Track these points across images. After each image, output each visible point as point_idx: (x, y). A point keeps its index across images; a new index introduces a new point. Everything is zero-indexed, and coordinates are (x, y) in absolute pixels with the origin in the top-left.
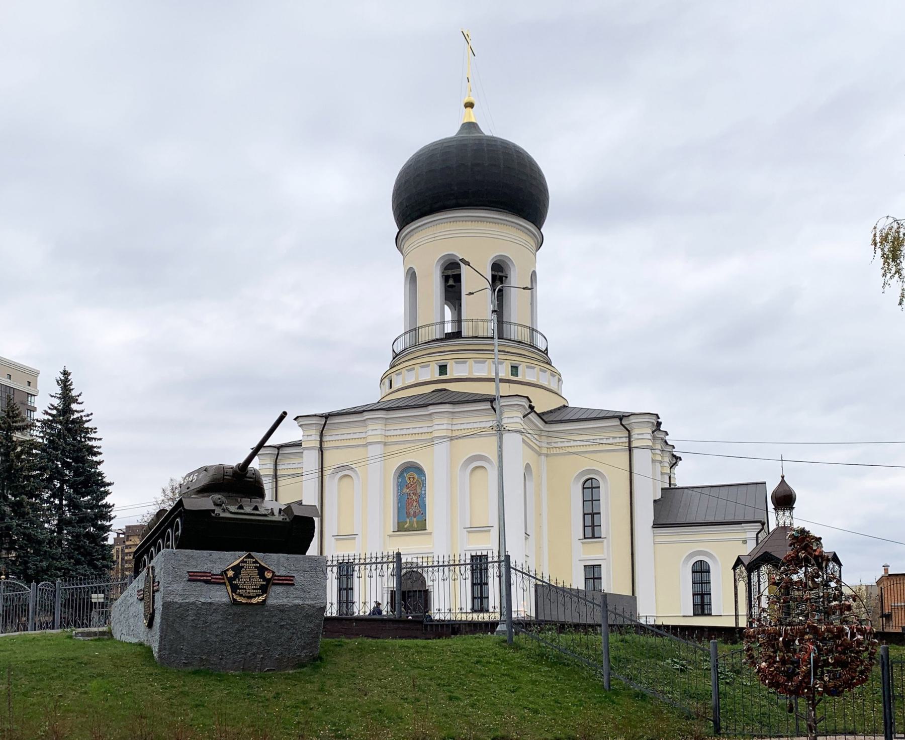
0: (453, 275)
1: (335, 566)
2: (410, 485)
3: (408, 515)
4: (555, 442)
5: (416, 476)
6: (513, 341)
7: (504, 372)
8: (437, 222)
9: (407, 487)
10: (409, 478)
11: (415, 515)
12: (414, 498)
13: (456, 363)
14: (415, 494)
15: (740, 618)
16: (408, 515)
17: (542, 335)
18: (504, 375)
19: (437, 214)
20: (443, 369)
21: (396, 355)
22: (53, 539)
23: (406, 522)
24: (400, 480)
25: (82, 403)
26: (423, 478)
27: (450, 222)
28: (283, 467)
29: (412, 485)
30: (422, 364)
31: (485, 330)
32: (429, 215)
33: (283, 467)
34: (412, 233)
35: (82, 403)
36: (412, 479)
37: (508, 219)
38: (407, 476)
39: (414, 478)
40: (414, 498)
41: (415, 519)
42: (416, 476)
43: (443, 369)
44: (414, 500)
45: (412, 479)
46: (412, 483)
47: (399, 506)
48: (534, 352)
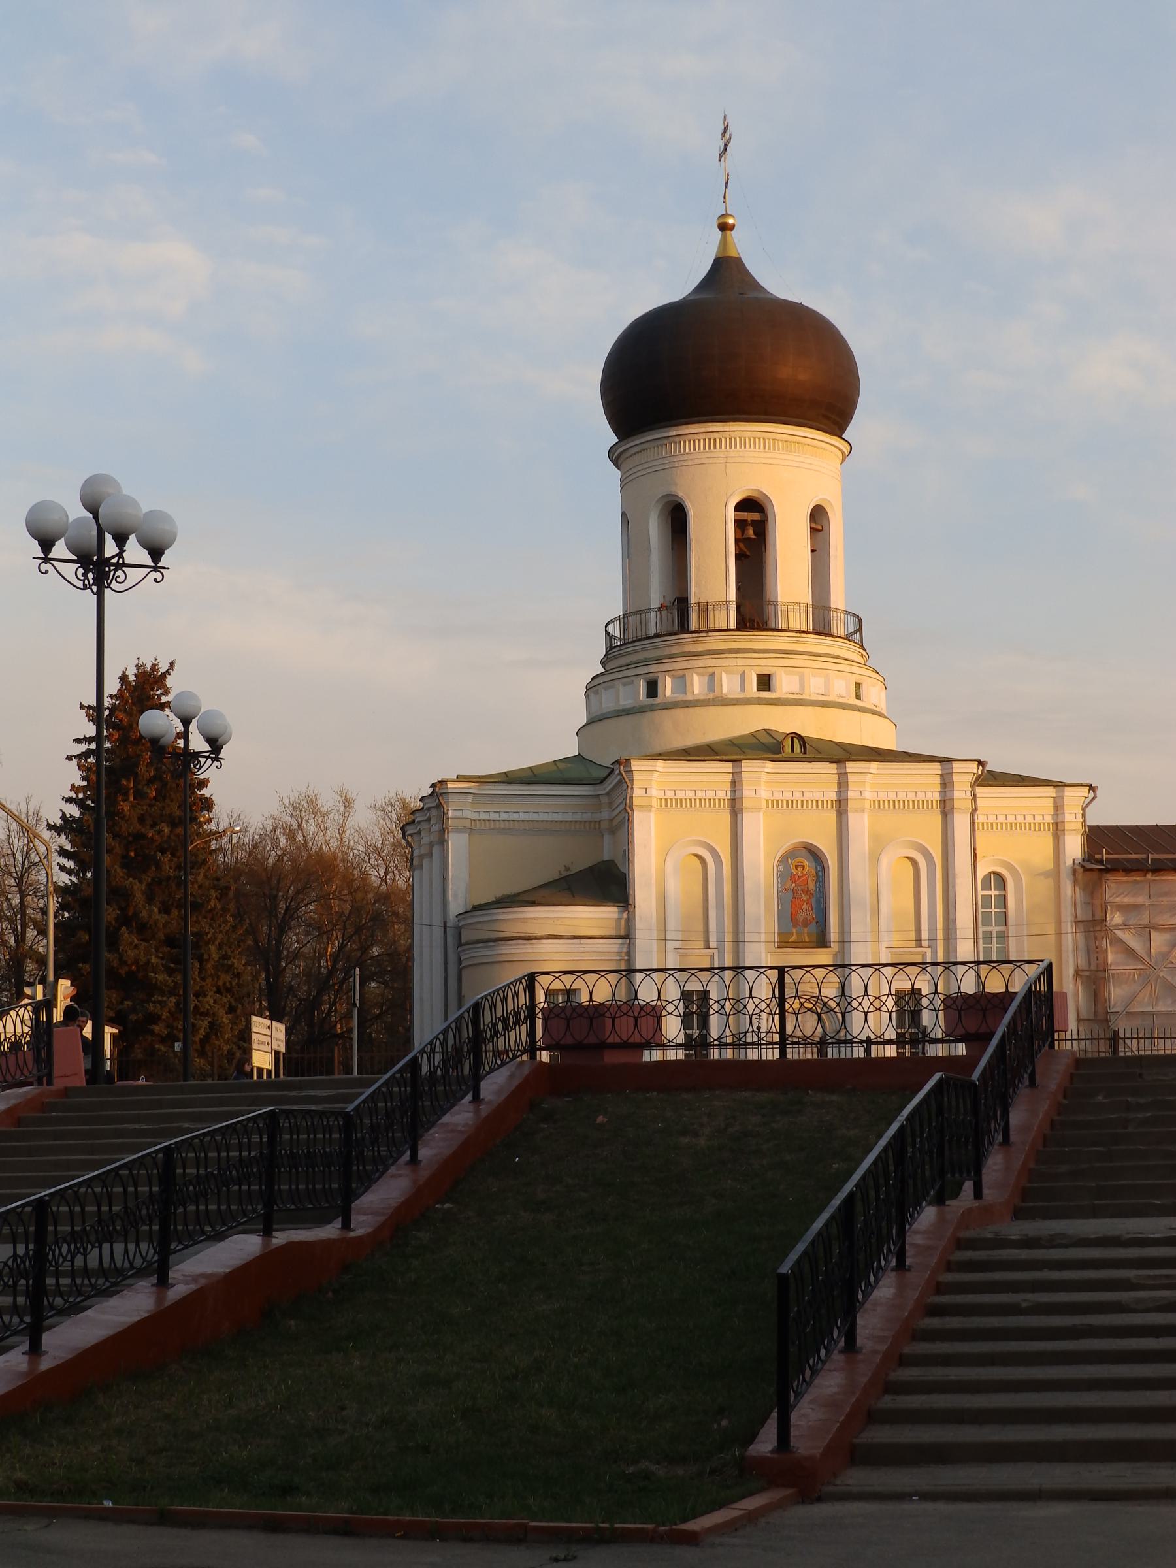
0: (752, 521)
1: (1057, 1040)
2: (797, 877)
4: (691, 459)
6: (837, 637)
10: (796, 867)
12: (805, 898)
16: (795, 922)
19: (635, 437)
25: (172, 665)
28: (780, 626)
31: (822, 625)
33: (780, 626)
35: (172, 665)
36: (800, 869)
39: (803, 867)
41: (806, 930)
42: (807, 864)
45: (800, 869)
46: (800, 874)
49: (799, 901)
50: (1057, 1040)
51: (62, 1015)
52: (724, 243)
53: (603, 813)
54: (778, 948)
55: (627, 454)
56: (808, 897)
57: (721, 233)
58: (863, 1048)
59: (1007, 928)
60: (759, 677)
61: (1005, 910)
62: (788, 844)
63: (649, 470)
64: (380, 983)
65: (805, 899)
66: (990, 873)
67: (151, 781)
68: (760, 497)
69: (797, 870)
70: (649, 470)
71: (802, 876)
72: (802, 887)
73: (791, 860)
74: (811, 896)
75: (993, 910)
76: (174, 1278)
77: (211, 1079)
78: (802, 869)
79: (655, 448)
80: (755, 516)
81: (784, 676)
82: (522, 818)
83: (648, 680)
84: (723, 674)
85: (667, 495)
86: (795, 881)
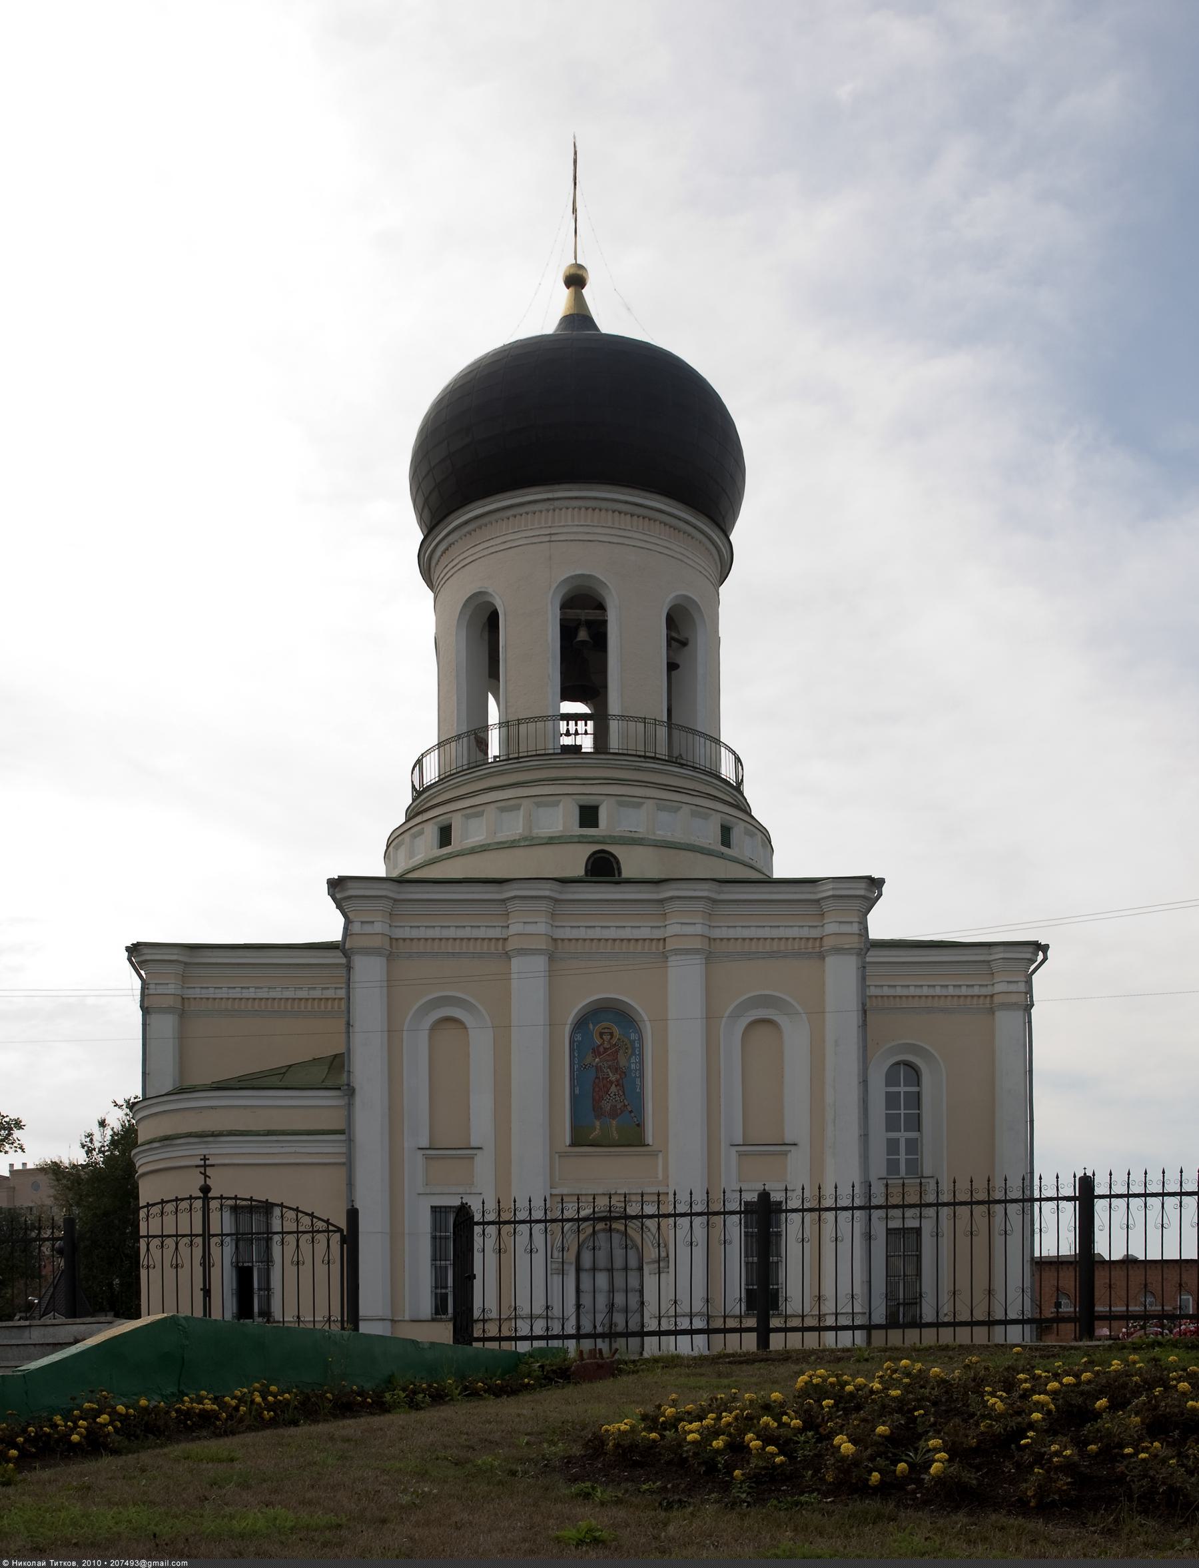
1: (478, 1223)
2: (602, 1049)
3: (598, 1112)
7: (709, 835)
8: (557, 503)
9: (596, 1052)
10: (601, 1034)
11: (614, 1114)
12: (613, 1077)
14: (616, 1070)
15: (528, 1343)
18: (482, 838)
20: (445, 835)
24: (579, 1037)
26: (633, 1036)
30: (540, 799)
32: (559, 483)
34: (486, 520)
37: (699, 524)
39: (612, 1034)
40: (613, 1077)
43: (445, 835)
44: (611, 1082)
46: (606, 1045)
47: (577, 1092)
49: (605, 1081)
50: (478, 1223)
51: (477, 1257)
56: (618, 1076)
58: (338, 1235)
59: (921, 1134)
61: (917, 1111)
63: (627, 541)
66: (898, 1063)
68: (562, 594)
70: (627, 541)
71: (610, 1048)
72: (610, 1063)
73: (594, 1026)
74: (623, 1076)
75: (902, 1112)
77: (112, 1313)
78: (609, 1037)
79: (543, 513)
86: (600, 1054)
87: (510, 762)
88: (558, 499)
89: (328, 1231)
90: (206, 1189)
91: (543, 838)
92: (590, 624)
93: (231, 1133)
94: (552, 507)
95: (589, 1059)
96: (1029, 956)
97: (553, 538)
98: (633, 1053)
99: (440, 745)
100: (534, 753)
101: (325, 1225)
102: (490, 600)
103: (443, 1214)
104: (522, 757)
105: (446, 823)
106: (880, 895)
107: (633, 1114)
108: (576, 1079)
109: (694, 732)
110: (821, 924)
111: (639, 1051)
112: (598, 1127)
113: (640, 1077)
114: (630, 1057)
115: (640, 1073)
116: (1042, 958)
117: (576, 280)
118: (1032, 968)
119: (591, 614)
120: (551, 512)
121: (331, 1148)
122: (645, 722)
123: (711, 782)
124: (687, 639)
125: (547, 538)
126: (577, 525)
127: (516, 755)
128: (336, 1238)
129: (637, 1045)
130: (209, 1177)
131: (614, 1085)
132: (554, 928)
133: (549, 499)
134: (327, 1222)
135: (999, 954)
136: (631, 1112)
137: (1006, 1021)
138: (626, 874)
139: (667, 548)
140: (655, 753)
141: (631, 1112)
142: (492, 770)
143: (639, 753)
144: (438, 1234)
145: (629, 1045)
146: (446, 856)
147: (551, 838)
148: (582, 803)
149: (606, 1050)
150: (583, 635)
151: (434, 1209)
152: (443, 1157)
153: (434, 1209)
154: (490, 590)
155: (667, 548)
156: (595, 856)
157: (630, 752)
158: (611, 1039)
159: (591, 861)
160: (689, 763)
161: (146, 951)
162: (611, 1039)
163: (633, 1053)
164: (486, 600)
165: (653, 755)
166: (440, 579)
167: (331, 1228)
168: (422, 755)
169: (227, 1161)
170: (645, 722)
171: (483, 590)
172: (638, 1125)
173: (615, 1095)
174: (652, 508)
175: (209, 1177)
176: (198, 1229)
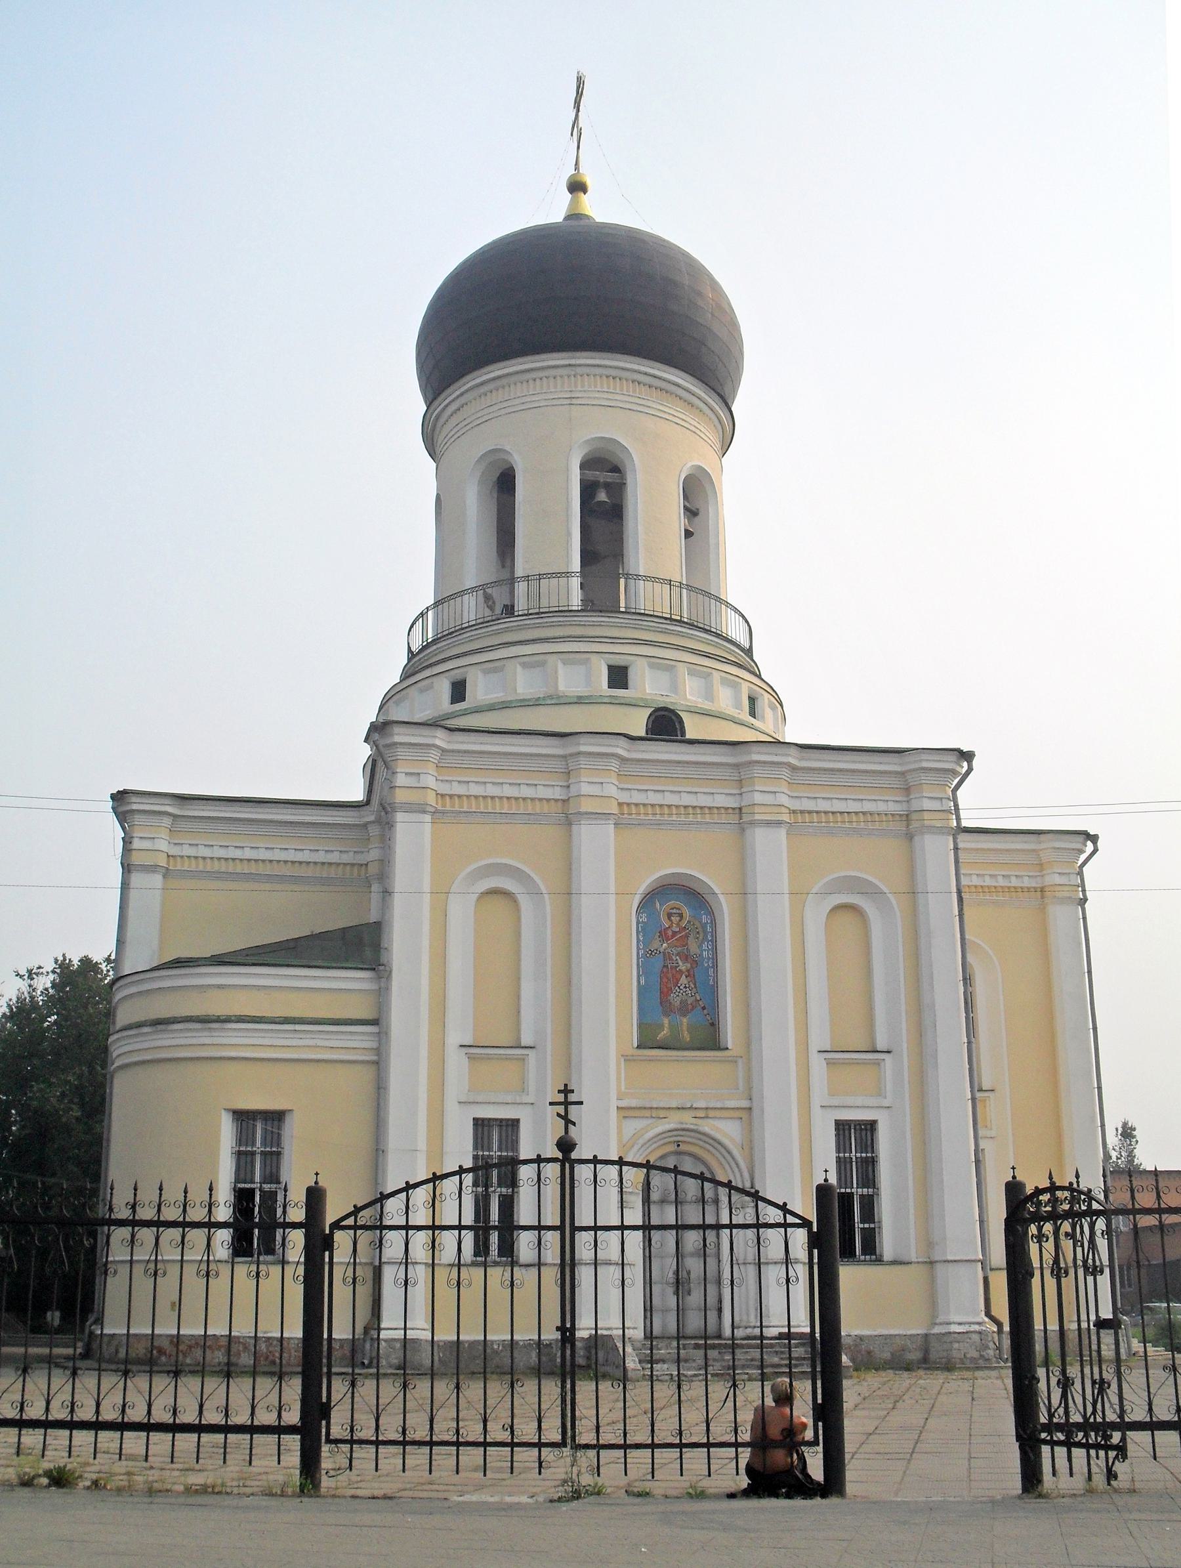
2: (670, 933)
5: (687, 912)
9: (663, 935)
10: (669, 916)
11: (684, 1010)
12: (683, 966)
13: (651, 666)
14: (686, 957)
17: (736, 610)
20: (459, 691)
21: (411, 655)
22: (60, 998)
23: (661, 1027)
24: (644, 918)
26: (704, 919)
27: (503, 387)
29: (674, 933)
36: (675, 919)
37: (710, 401)
38: (661, 908)
39: (681, 916)
40: (683, 966)
42: (687, 912)
43: (459, 691)
45: (675, 919)
47: (643, 982)
48: (716, 646)
52: (574, 203)
53: (371, 851)
54: (638, 1047)
55: (442, 420)
57: (570, 196)
60: (611, 668)
62: (648, 881)
64: (950, 1333)
65: (683, 968)
67: (1086, 1436)
69: (671, 921)
71: (679, 932)
76: (243, 1454)
78: (678, 919)
80: (610, 477)
81: (647, 671)
82: (231, 855)
83: (452, 680)
84: (560, 665)
85: (490, 451)
86: (668, 939)
87: (531, 617)
88: (580, 365)
89: (785, 1225)
90: (566, 1146)
91: (570, 697)
92: (607, 486)
93: (241, 1019)
94: (573, 373)
95: (656, 944)
96: (1079, 846)
97: (574, 401)
98: (705, 939)
99: (437, 604)
100: (557, 609)
101: (780, 1213)
102: (510, 459)
103: (486, 1128)
104: (543, 613)
105: (459, 678)
106: (970, 770)
107: (705, 1011)
108: (644, 969)
109: (718, 599)
110: (367, 850)
111: (712, 936)
112: (666, 1025)
113: (713, 967)
114: (702, 942)
115: (713, 963)
116: (1092, 849)
117: (577, 187)
118: (1083, 857)
119: (610, 477)
120: (572, 377)
121: (359, 1040)
122: (670, 584)
123: (734, 651)
124: (698, 509)
125: (568, 401)
126: (607, 392)
127: (537, 611)
128: (799, 1237)
129: (709, 929)
130: (574, 1124)
131: (684, 976)
132: (620, 790)
133: (570, 365)
134: (783, 1208)
135: (1047, 843)
136: (704, 1008)
137: (1059, 915)
138: (689, 735)
139: (683, 420)
140: (681, 616)
141: (704, 1008)
142: (512, 624)
143: (664, 615)
144: (841, 1155)
145: (700, 930)
146: (461, 713)
147: (580, 697)
148: (612, 663)
149: (674, 933)
150: (602, 496)
151: (479, 1123)
152: (489, 1058)
153: (479, 1123)
154: (508, 448)
155: (683, 420)
156: (656, 714)
157: (656, 614)
158: (680, 921)
159: (652, 718)
160: (713, 630)
161: (134, 799)
162: (680, 921)
163: (705, 939)
164: (506, 458)
165: (679, 618)
166: (448, 437)
167: (791, 1219)
168: (427, 608)
169: (233, 1054)
170: (670, 584)
171: (498, 447)
172: (712, 1024)
173: (685, 987)
174: (670, 382)
175: (574, 1124)
176: (551, 1217)
